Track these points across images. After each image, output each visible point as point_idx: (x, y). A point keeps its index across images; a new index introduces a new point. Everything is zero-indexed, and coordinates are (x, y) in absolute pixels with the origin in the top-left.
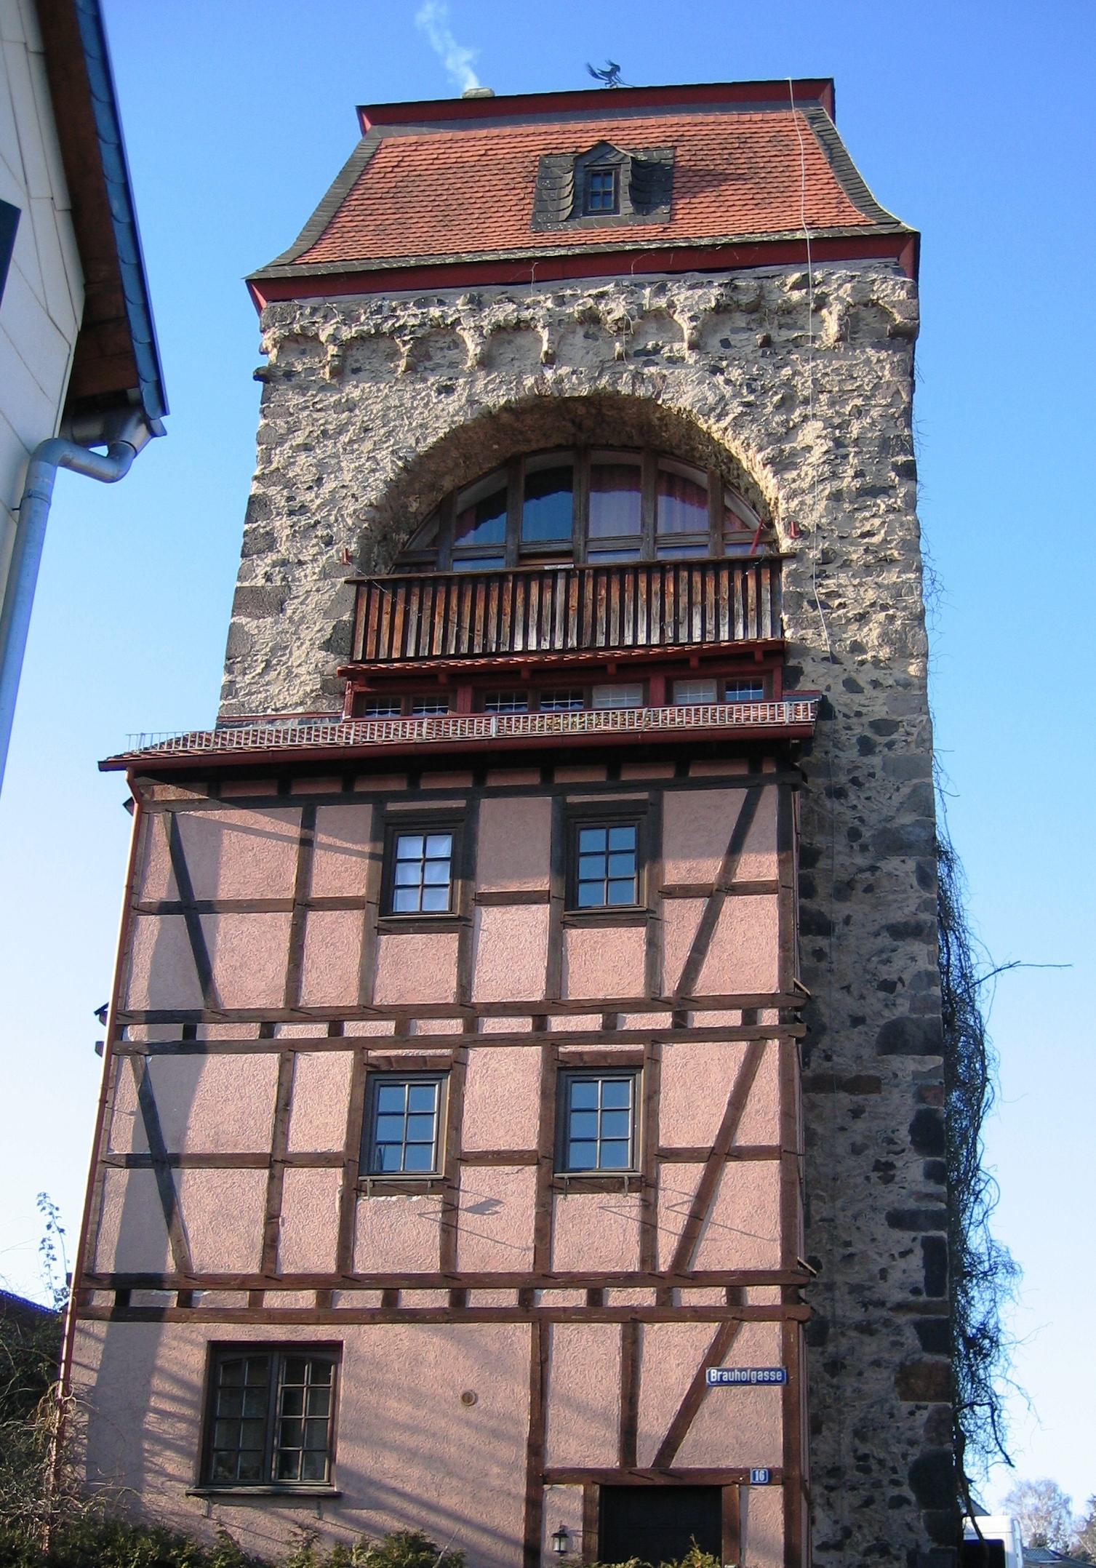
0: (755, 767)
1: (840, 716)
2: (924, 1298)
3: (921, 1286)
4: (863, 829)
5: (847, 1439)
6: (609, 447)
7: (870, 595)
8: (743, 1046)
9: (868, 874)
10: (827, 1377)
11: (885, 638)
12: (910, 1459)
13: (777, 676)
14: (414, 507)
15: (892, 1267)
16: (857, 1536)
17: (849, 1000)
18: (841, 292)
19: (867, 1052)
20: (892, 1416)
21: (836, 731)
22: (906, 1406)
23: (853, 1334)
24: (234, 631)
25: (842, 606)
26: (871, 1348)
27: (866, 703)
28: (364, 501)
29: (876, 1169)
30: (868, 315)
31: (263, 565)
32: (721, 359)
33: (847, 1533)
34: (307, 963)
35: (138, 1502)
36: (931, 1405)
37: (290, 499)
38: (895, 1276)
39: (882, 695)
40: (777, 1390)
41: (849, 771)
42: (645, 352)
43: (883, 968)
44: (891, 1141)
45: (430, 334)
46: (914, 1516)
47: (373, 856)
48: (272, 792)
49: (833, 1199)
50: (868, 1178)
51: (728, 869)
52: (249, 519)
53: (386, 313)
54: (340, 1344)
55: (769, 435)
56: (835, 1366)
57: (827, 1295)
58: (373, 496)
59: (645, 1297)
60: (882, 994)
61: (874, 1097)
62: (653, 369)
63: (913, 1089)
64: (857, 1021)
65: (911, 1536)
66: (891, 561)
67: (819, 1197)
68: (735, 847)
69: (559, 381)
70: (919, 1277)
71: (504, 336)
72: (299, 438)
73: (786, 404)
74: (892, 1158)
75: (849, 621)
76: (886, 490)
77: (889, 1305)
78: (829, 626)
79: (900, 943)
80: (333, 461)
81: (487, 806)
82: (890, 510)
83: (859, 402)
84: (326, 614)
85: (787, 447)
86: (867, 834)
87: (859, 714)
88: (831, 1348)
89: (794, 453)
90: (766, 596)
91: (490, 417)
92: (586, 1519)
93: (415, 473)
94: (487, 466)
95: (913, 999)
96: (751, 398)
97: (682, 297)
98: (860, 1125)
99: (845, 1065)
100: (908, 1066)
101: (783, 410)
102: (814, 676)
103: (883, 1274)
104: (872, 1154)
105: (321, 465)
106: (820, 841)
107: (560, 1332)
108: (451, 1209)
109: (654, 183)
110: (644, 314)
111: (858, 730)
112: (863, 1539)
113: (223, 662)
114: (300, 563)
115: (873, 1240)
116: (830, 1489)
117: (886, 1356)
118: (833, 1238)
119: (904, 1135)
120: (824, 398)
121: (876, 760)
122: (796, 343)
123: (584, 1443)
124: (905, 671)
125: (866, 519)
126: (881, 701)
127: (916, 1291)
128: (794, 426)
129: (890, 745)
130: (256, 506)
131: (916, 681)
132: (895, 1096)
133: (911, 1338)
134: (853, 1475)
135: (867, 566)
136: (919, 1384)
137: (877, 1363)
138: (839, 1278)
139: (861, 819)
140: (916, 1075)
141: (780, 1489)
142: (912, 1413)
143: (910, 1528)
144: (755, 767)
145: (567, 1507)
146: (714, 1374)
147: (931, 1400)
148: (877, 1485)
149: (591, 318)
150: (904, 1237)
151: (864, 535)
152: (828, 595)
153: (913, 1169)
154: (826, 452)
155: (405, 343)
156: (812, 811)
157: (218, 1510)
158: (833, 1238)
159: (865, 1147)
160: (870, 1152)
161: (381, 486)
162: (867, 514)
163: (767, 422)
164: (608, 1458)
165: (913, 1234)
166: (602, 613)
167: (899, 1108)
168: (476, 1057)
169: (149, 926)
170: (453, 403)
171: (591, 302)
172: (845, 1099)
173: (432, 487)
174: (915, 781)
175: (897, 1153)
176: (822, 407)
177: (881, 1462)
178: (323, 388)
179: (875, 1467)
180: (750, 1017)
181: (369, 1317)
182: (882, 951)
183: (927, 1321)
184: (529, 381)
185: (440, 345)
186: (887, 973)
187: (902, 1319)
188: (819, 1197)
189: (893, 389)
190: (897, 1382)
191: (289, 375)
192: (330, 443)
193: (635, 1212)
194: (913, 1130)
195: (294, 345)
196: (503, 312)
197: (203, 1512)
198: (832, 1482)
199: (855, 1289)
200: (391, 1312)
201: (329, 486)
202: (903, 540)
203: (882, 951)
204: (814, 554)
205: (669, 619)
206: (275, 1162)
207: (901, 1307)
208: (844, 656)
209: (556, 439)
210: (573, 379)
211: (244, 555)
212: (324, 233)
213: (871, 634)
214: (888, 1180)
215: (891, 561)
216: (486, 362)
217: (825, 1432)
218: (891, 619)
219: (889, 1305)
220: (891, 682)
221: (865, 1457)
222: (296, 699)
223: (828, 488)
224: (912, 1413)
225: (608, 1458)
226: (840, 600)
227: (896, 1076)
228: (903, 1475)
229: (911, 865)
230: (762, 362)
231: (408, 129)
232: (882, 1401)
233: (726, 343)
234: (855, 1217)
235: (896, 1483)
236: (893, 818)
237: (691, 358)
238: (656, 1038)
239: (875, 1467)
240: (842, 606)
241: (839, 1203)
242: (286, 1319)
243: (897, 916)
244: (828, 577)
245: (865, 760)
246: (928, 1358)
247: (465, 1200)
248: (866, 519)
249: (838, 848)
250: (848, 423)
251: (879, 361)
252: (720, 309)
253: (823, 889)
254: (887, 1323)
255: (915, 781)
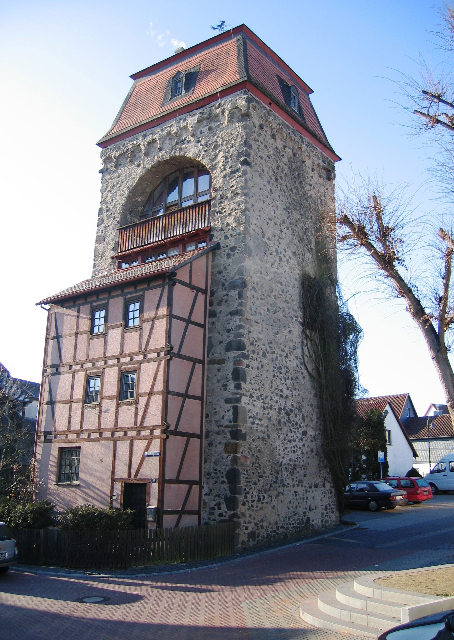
0: (164, 281)
1: (222, 248)
2: (232, 424)
3: (232, 420)
4: (226, 283)
5: (212, 464)
6: (187, 168)
7: (232, 207)
8: (157, 363)
9: (226, 297)
10: (208, 447)
11: (235, 220)
12: (227, 470)
13: (208, 238)
14: (140, 200)
15: (226, 415)
16: (213, 492)
17: (219, 336)
18: (228, 107)
19: (223, 352)
20: (223, 458)
21: (221, 253)
22: (226, 455)
23: (215, 435)
24: (96, 248)
25: (225, 212)
26: (219, 438)
27: (229, 242)
28: (121, 204)
29: (223, 386)
30: (236, 111)
31: (102, 228)
32: (200, 138)
33: (211, 491)
34: (77, 349)
35: (47, 487)
36: (232, 455)
37: (107, 207)
38: (226, 417)
39: (233, 239)
40: (158, 457)
41: (224, 265)
42: (183, 141)
43: (228, 325)
44: (227, 378)
45: (135, 149)
46: (226, 486)
47: (90, 319)
48: (72, 304)
49: (213, 395)
50: (221, 389)
51: (156, 313)
52: (99, 216)
53: (125, 145)
54: (80, 447)
55: (210, 160)
56: (210, 444)
57: (210, 424)
58: (123, 202)
59: (134, 433)
60: (227, 334)
61: (223, 365)
62: (184, 146)
63: (233, 362)
64: (221, 342)
65: (225, 492)
66: (238, 194)
67: (209, 396)
68: (158, 307)
69: (162, 156)
70: (231, 417)
71: (151, 145)
72: (109, 189)
73: (215, 148)
74: (227, 383)
75: (226, 216)
76: (237, 171)
77: (224, 426)
78: (221, 219)
79: (232, 317)
80: (115, 194)
81: (111, 301)
82: (239, 177)
83: (233, 142)
84: (113, 240)
85: (214, 163)
86: (227, 284)
87: (227, 246)
88: (210, 439)
89: (216, 165)
90: (207, 213)
91: (149, 171)
92: (121, 491)
93: (133, 192)
94: (159, 182)
95: (235, 334)
96: (206, 149)
97: (189, 121)
98: (220, 374)
99: (217, 356)
100: (232, 354)
101: (214, 150)
102: (216, 236)
103: (223, 417)
104: (222, 382)
105: (113, 196)
106: (215, 288)
107: (119, 443)
108: (100, 412)
109: (191, 79)
110: (181, 129)
111: (227, 251)
112: (215, 492)
113: (93, 258)
114: (109, 226)
115: (221, 407)
116: (208, 478)
117: (222, 441)
118: (212, 407)
119: (230, 376)
120: (224, 143)
121: (230, 260)
122: (218, 126)
123: (122, 472)
124: (240, 230)
125: (232, 181)
126: (233, 241)
127: (230, 422)
128: (217, 155)
129: (234, 255)
130: (101, 210)
131: (242, 232)
132: (228, 365)
133: (228, 435)
134: (213, 475)
135: (232, 197)
136: (229, 449)
137: (220, 443)
138: (213, 419)
139: (226, 280)
140: (234, 357)
141: (158, 484)
142: (227, 457)
143: (225, 489)
144: (164, 281)
145: (118, 487)
146: (146, 453)
147: (232, 453)
148: (218, 477)
149: (169, 134)
150: (228, 406)
151: (231, 187)
152: (221, 209)
153: (231, 385)
154: (223, 162)
155: (129, 154)
156: (214, 279)
157: (60, 489)
158: (212, 407)
159: (221, 380)
160: (221, 381)
161: (125, 198)
162: (232, 180)
163: (210, 155)
164: (125, 476)
165: (230, 405)
166: (170, 227)
167: (229, 367)
168: (107, 370)
169: (51, 342)
170: (140, 169)
171: (169, 128)
172: (216, 366)
173: (143, 193)
174: (239, 265)
175: (228, 381)
176: (224, 147)
177: (220, 471)
178: (114, 172)
179: (218, 472)
180: (159, 354)
181: (86, 440)
182: (227, 321)
183: (232, 430)
184: (156, 158)
185: (138, 151)
186: (229, 327)
187: (227, 430)
188: (209, 396)
189: (242, 135)
190: (224, 448)
191: (107, 170)
192: (115, 188)
193: (134, 411)
194: (232, 374)
195: (108, 160)
196: (150, 138)
197: (57, 489)
198: (208, 477)
199: (217, 422)
200: (89, 439)
201: (114, 201)
202: (241, 186)
203: (227, 321)
204: (219, 197)
205: (184, 225)
206: (70, 402)
207: (227, 427)
208: (224, 228)
209: (174, 170)
210: (165, 155)
211: (98, 226)
212: (117, 122)
213: (230, 220)
214: (226, 389)
215: (238, 194)
216: (147, 155)
217: (207, 463)
218: (236, 213)
219: (224, 426)
220: (235, 234)
221: (216, 470)
222: (107, 266)
223: (223, 174)
224: (227, 457)
225: (125, 476)
226: (224, 210)
227: (229, 358)
228: (224, 475)
229: (237, 292)
230: (210, 135)
231: (140, 79)
232: (221, 454)
233: (201, 132)
234: (217, 401)
235: (223, 477)
236: (233, 278)
237: (192, 139)
238: (140, 363)
239: (218, 472)
240: (225, 212)
241: (214, 397)
242: (71, 441)
243: (232, 309)
244: (222, 203)
245: (228, 261)
246: (232, 441)
247: (103, 409)
248: (232, 181)
249: (220, 290)
250: (229, 150)
251: (239, 126)
252: (199, 121)
253: (215, 303)
254: (223, 431)
255: (239, 265)
